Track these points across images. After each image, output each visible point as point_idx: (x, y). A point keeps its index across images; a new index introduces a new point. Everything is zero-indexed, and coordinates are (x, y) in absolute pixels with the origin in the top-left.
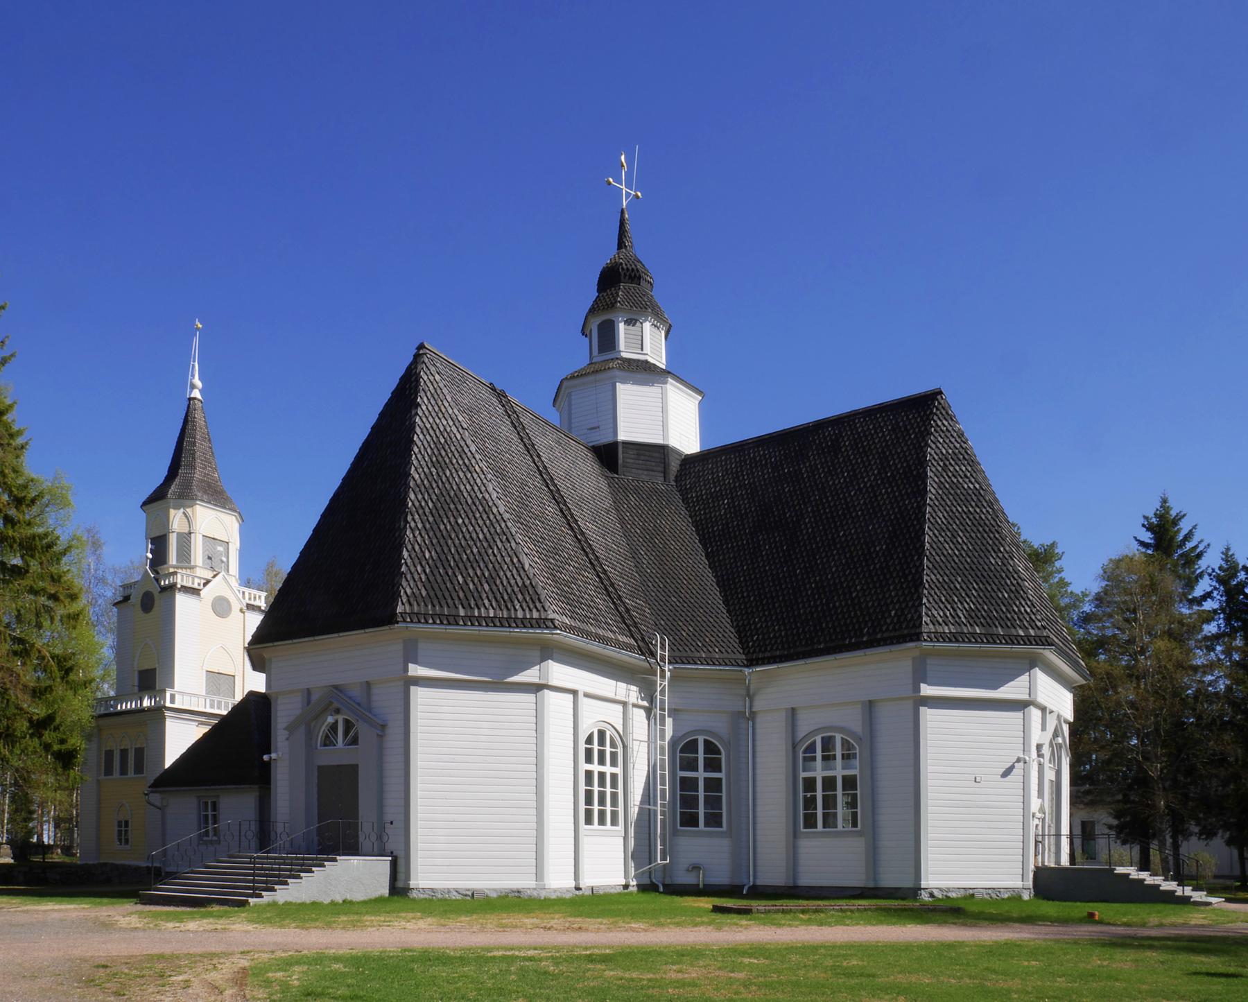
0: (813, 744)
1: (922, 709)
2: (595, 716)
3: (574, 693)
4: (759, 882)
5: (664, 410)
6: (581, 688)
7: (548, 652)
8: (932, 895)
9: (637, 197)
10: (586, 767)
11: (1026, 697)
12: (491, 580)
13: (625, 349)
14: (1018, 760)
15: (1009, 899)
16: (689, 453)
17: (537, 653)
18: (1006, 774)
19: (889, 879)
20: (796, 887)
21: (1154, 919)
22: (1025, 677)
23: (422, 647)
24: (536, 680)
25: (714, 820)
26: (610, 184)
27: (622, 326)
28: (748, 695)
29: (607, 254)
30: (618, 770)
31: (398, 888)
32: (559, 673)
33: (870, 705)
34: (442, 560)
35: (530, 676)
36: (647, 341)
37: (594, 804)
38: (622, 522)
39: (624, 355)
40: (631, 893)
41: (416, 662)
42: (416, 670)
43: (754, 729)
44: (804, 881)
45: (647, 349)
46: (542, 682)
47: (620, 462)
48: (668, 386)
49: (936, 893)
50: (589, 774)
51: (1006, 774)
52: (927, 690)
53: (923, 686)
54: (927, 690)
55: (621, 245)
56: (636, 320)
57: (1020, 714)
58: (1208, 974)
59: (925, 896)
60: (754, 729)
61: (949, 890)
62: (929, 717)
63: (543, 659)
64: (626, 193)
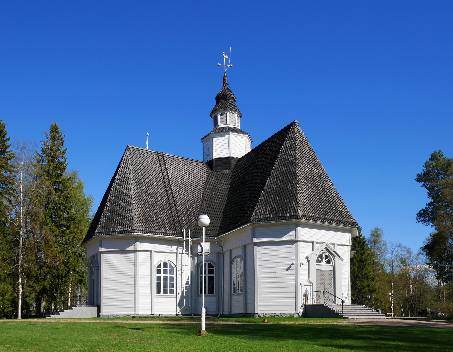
0: (160, 264)
1: (255, 247)
2: (158, 259)
3: (151, 251)
4: (224, 313)
5: (229, 144)
6: (153, 250)
7: (138, 239)
8: (259, 316)
9: (231, 66)
10: (174, 276)
11: (294, 239)
12: (122, 220)
13: (221, 125)
14: (293, 264)
15: (290, 317)
16: (240, 157)
17: (134, 240)
18: (288, 269)
19: (249, 311)
20: (231, 314)
21: (306, 322)
22: (294, 231)
23: (103, 242)
24: (133, 249)
25: (172, 292)
26: (219, 65)
27: (219, 116)
28: (221, 246)
29: (218, 90)
30: (174, 276)
31: (99, 315)
32: (140, 246)
33: (245, 246)
34: (111, 215)
35: (132, 248)
36: (231, 119)
37: (162, 287)
38: (205, 189)
39: (220, 126)
40: (180, 317)
41: (101, 247)
42: (102, 249)
43: (224, 258)
44: (233, 312)
45: (228, 122)
46: (135, 249)
47: (214, 165)
48: (230, 135)
49: (261, 315)
50: (159, 278)
51: (288, 269)
52: (256, 240)
53: (254, 239)
54: (256, 240)
55: (224, 86)
56: (224, 113)
57: (294, 246)
58: (137, 329)
59: (257, 316)
60: (224, 258)
61: (266, 314)
62: (258, 250)
63: (136, 242)
64: (226, 67)
